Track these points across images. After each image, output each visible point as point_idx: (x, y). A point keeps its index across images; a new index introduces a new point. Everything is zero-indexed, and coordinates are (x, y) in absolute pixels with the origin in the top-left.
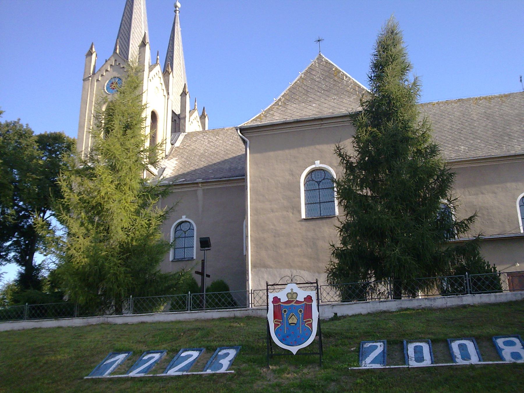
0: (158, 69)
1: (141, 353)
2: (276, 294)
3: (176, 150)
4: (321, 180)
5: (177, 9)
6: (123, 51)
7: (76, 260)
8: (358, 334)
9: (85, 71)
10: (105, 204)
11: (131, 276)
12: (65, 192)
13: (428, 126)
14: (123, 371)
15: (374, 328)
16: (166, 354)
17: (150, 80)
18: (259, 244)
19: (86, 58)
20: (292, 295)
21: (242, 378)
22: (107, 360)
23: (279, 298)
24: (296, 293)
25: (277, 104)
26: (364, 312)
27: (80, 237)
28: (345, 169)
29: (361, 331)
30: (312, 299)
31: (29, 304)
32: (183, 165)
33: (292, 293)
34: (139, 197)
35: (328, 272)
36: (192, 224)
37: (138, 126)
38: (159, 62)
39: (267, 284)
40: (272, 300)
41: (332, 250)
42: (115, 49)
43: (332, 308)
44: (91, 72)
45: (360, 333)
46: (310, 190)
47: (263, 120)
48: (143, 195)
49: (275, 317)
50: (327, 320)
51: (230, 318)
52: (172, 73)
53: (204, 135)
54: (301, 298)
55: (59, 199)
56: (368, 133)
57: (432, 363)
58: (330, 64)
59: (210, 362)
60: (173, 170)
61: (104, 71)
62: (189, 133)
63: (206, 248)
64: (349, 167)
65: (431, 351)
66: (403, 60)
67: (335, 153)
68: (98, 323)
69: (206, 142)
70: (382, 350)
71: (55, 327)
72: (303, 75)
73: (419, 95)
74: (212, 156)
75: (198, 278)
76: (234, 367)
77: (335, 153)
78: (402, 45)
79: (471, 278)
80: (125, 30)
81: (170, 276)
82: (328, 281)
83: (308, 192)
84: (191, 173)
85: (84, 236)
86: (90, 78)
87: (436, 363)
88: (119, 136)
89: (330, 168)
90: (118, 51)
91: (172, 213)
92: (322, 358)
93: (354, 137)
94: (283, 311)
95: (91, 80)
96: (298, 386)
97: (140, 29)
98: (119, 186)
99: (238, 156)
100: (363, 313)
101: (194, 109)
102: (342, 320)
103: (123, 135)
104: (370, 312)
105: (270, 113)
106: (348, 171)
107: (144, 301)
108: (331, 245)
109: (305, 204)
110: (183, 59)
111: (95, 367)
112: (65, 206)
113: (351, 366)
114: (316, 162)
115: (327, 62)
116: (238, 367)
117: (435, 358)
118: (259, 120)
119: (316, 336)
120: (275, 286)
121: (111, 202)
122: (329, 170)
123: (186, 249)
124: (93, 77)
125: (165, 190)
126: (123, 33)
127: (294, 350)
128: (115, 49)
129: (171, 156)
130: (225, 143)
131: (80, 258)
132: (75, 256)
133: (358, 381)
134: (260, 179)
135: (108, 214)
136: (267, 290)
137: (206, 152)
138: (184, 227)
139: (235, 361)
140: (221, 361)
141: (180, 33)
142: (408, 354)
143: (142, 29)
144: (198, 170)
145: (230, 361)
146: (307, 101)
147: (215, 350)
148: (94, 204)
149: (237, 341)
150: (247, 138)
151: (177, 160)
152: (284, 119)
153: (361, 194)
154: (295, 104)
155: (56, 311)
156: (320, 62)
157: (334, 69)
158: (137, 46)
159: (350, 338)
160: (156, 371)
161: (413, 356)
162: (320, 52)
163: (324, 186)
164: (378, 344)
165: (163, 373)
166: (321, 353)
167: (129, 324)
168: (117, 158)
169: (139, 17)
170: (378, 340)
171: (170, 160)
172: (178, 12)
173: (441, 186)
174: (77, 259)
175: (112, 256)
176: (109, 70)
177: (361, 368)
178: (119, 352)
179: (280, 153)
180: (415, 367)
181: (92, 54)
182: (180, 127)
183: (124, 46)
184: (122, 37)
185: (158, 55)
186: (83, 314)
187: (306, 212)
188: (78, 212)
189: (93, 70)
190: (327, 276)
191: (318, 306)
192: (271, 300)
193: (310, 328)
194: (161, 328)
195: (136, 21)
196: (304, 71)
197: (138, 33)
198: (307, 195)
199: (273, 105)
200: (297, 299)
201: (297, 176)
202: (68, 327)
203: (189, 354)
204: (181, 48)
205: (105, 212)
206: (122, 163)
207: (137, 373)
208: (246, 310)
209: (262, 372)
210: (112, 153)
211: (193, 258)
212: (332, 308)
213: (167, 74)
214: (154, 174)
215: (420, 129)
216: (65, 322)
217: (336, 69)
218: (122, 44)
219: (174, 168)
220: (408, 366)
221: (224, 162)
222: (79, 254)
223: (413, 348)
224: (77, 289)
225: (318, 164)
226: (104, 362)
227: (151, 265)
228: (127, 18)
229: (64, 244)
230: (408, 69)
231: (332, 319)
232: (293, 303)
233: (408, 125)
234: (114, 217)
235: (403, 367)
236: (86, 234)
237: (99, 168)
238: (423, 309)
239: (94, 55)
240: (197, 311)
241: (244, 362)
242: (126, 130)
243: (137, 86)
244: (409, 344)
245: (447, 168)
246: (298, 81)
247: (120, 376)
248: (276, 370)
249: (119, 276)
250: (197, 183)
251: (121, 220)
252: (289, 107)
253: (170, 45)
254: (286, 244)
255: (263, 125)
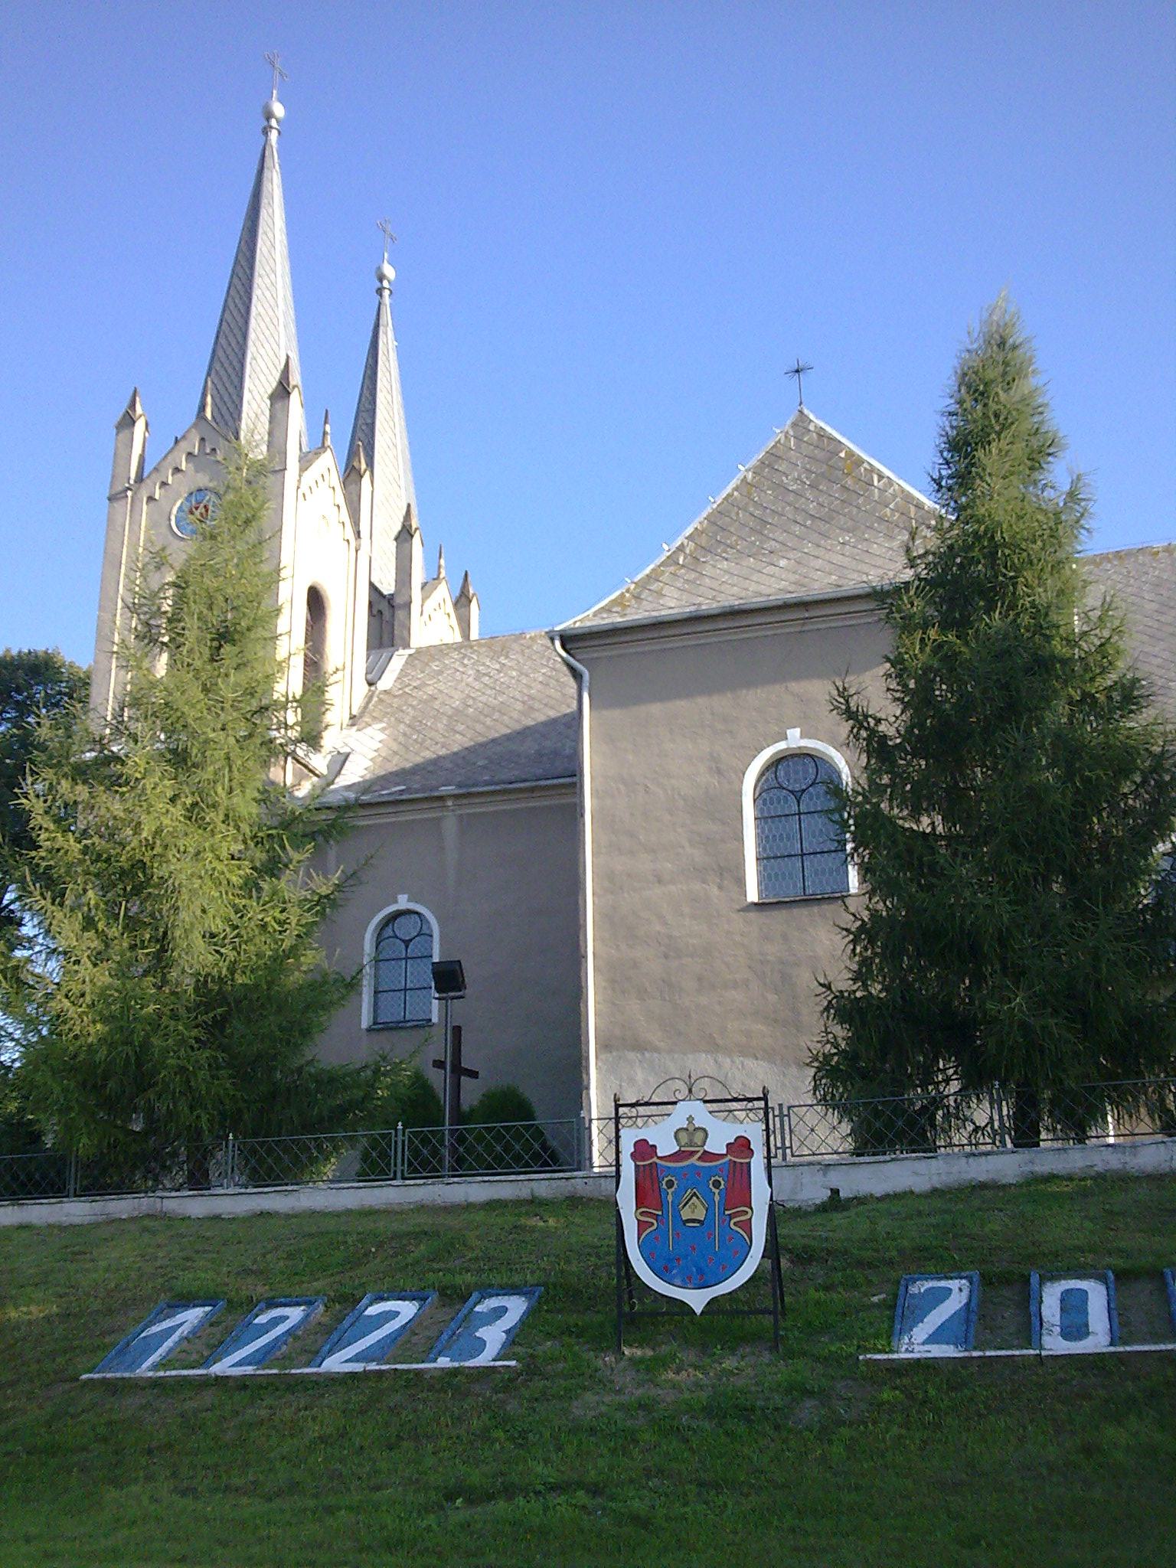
0: (328, 464)
1: (251, 1305)
2: (642, 1135)
3: (381, 700)
4: (804, 787)
5: (386, 284)
6: (224, 411)
7: (70, 1030)
8: (894, 1253)
9: (113, 470)
10: (156, 865)
11: (231, 1077)
12: (40, 829)
13: (1117, 623)
14: (194, 1357)
15: (944, 1234)
16: (322, 1308)
17: (304, 495)
18: (617, 979)
19: (117, 434)
20: (691, 1133)
21: (539, 1384)
22: (152, 1323)
23: (651, 1143)
24: (704, 1130)
25: (672, 560)
26: (921, 1185)
27: (82, 961)
28: (865, 755)
29: (906, 1243)
30: (752, 1147)
31: (405, 1127)
32: (400, 743)
33: (691, 1129)
34: (257, 844)
35: (816, 1064)
36: (428, 922)
37: (260, 632)
38: (328, 442)
39: (615, 1101)
40: (633, 1150)
41: (825, 998)
42: (202, 407)
43: (825, 1175)
44: (133, 475)
45: (901, 1251)
46: (778, 816)
47: (628, 611)
48: (269, 835)
49: (641, 1200)
50: (809, 1209)
51: (518, 1203)
52: (368, 473)
53: (465, 656)
54: (716, 1144)
55: (23, 852)
56: (928, 649)
57: (1111, 1345)
58: (831, 439)
59: (450, 1333)
60: (371, 760)
61: (170, 471)
62: (419, 651)
63: (452, 994)
64: (878, 750)
65: (1112, 1306)
66: (1036, 426)
67: (832, 710)
68: (136, 1213)
69: (470, 676)
70: (965, 1301)
71: (12, 1226)
72: (750, 473)
73: (1088, 530)
74: (486, 716)
75: (437, 1079)
76: (518, 1349)
77: (832, 710)
78: (1033, 382)
79: (409, 1137)
80: (229, 351)
81: (345, 1075)
82: (814, 1094)
83: (766, 823)
84: (424, 769)
85: (93, 959)
86: (129, 493)
87: (1125, 1343)
88: (198, 664)
89: (831, 748)
90: (208, 414)
91: (354, 889)
92: (782, 1324)
93: (888, 660)
94: (664, 1183)
95: (132, 497)
96: (704, 1409)
97: (275, 346)
98: (196, 810)
99: (565, 715)
100: (917, 1190)
101: (434, 579)
102: (852, 1212)
103: (212, 660)
104: (938, 1186)
105: (651, 588)
106: (873, 761)
107: (270, 1151)
108: (821, 985)
109: (757, 859)
110: (405, 434)
111: (114, 1345)
112: (41, 871)
113: (867, 1350)
114: (788, 732)
115: (821, 434)
116: (531, 1351)
117: (1121, 1326)
118: (618, 609)
119: (763, 1257)
120: (640, 1108)
121: (171, 857)
122: (831, 758)
123: (408, 992)
124: (139, 488)
125: (334, 820)
126: (223, 359)
127: (697, 1300)
128: (202, 407)
129: (367, 719)
130: (527, 676)
131: (82, 1021)
132: (69, 1015)
133: (886, 1395)
134: (622, 787)
135: (162, 892)
136: (617, 1118)
137: (469, 706)
138: (405, 928)
139: (522, 1330)
140: (481, 1333)
141: (393, 356)
142: (1043, 1314)
143: (278, 346)
144: (444, 758)
145: (507, 1332)
146: (763, 551)
147: (464, 1299)
148: (126, 866)
149: (533, 1272)
150: (581, 663)
151: (383, 730)
152: (694, 604)
153: (915, 827)
154: (726, 559)
155: (15, 1178)
156: (803, 434)
157: (842, 455)
158: (266, 396)
159: (870, 1265)
160: (287, 1360)
161: (1057, 1320)
162: (801, 404)
163: (815, 804)
164: (953, 1284)
165: (308, 1365)
166: (780, 1311)
167: (223, 1219)
168: (191, 730)
169: (271, 313)
170: (952, 1270)
171: (364, 731)
172: (386, 293)
173: (1155, 802)
174: (74, 1025)
175: (174, 1016)
176: (183, 467)
177: (895, 1356)
178: (186, 1301)
179: (681, 705)
180: (1059, 1353)
181: (134, 422)
182: (396, 632)
183: (226, 398)
184: (222, 372)
185: (326, 422)
186: (94, 1188)
187: (759, 883)
188: (76, 887)
189: (138, 468)
190: (814, 1077)
191: (769, 1167)
192: (627, 1147)
193: (744, 1234)
194: (314, 1230)
195: (262, 324)
196: (753, 462)
197: (265, 358)
198: (763, 832)
199: (659, 566)
200: (706, 1148)
201: (733, 776)
202: (50, 1226)
203: (387, 1309)
204: (398, 398)
205: (158, 886)
206: (207, 741)
207: (233, 1366)
208: (567, 1179)
209: (600, 1363)
210: (179, 714)
211: (430, 1020)
212: (825, 1175)
213: (353, 476)
214: (317, 772)
215: (1092, 630)
216: (40, 1213)
217: (851, 454)
218: (222, 391)
219: (376, 754)
220: (1038, 1352)
221: (524, 733)
222: (80, 1010)
223: (1059, 1295)
224: (73, 1115)
225: (795, 739)
226: (142, 1332)
227: (288, 1043)
228: (235, 314)
229: (38, 982)
230: (1051, 450)
231: (823, 1208)
232: (694, 1160)
233: (1048, 619)
234: (179, 903)
235: (1023, 1356)
236: (99, 953)
237: (136, 759)
238: (1100, 1177)
239: (140, 427)
240: (421, 1181)
241: (549, 1335)
242: (221, 646)
243: (253, 516)
244: (1049, 1284)
245: (1171, 748)
246: (736, 493)
247: (185, 1372)
248: (641, 1360)
249: (195, 1075)
250: (441, 798)
251: (204, 911)
252: (708, 570)
253: (365, 391)
254: (700, 979)
255: (630, 624)
